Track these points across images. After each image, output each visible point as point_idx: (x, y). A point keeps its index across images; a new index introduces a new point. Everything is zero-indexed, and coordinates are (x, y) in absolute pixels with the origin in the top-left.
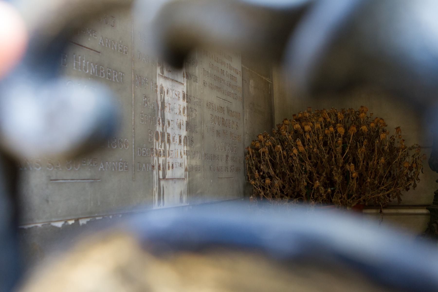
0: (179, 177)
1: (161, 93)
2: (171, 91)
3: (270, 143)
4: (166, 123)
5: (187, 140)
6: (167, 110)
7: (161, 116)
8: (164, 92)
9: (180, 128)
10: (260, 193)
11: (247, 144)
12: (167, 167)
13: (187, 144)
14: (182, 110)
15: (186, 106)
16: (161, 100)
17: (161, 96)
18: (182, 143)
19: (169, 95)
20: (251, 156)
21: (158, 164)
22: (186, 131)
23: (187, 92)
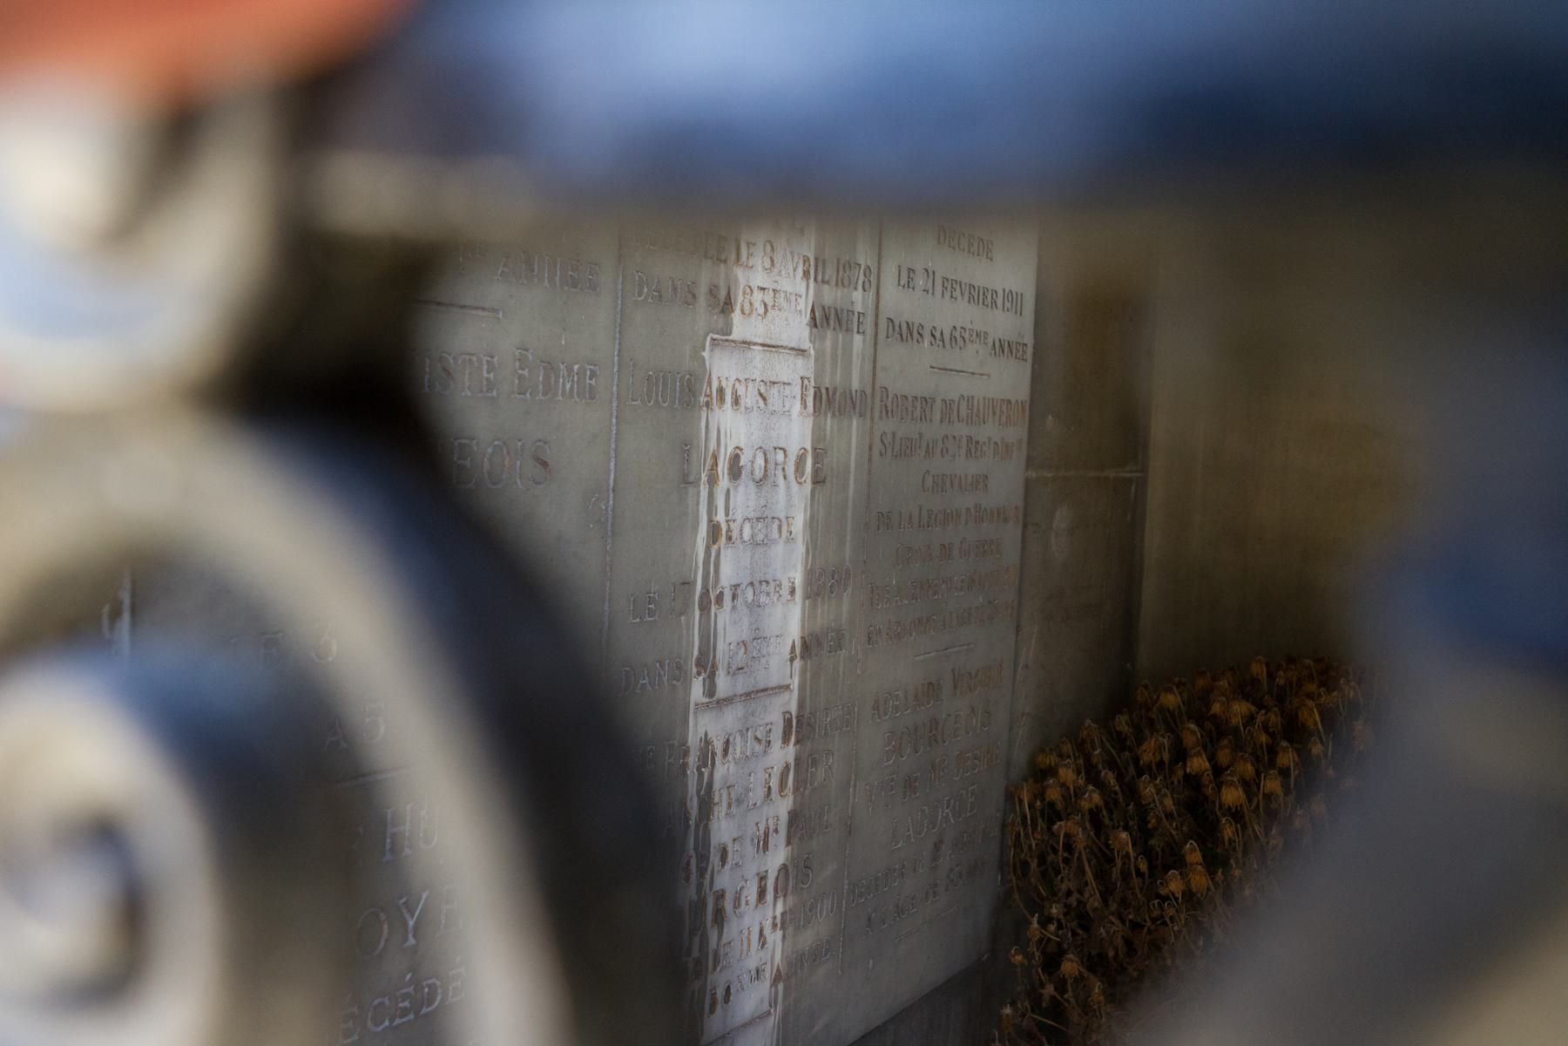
0: (793, 345)
1: (699, 769)
2: (738, 739)
3: (1097, 798)
4: (715, 859)
5: (787, 879)
6: (720, 811)
7: (696, 849)
8: (714, 754)
9: (766, 848)
10: (1042, 985)
11: (1020, 757)
12: (707, 1007)
13: (785, 889)
14: (774, 784)
15: (791, 760)
16: (698, 792)
17: (701, 774)
18: (770, 896)
19: (730, 757)
20: (1025, 817)
21: (710, 520)
22: (788, 843)
23: (801, 705)
